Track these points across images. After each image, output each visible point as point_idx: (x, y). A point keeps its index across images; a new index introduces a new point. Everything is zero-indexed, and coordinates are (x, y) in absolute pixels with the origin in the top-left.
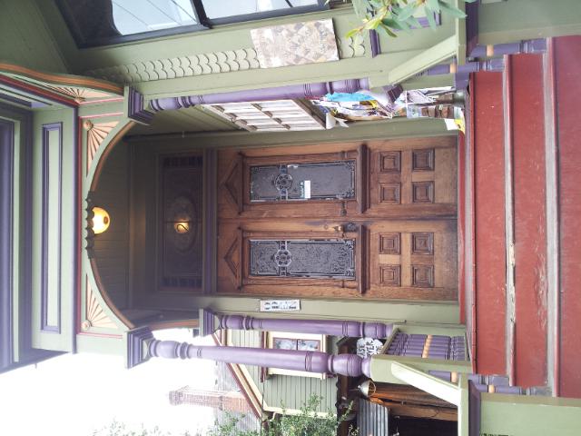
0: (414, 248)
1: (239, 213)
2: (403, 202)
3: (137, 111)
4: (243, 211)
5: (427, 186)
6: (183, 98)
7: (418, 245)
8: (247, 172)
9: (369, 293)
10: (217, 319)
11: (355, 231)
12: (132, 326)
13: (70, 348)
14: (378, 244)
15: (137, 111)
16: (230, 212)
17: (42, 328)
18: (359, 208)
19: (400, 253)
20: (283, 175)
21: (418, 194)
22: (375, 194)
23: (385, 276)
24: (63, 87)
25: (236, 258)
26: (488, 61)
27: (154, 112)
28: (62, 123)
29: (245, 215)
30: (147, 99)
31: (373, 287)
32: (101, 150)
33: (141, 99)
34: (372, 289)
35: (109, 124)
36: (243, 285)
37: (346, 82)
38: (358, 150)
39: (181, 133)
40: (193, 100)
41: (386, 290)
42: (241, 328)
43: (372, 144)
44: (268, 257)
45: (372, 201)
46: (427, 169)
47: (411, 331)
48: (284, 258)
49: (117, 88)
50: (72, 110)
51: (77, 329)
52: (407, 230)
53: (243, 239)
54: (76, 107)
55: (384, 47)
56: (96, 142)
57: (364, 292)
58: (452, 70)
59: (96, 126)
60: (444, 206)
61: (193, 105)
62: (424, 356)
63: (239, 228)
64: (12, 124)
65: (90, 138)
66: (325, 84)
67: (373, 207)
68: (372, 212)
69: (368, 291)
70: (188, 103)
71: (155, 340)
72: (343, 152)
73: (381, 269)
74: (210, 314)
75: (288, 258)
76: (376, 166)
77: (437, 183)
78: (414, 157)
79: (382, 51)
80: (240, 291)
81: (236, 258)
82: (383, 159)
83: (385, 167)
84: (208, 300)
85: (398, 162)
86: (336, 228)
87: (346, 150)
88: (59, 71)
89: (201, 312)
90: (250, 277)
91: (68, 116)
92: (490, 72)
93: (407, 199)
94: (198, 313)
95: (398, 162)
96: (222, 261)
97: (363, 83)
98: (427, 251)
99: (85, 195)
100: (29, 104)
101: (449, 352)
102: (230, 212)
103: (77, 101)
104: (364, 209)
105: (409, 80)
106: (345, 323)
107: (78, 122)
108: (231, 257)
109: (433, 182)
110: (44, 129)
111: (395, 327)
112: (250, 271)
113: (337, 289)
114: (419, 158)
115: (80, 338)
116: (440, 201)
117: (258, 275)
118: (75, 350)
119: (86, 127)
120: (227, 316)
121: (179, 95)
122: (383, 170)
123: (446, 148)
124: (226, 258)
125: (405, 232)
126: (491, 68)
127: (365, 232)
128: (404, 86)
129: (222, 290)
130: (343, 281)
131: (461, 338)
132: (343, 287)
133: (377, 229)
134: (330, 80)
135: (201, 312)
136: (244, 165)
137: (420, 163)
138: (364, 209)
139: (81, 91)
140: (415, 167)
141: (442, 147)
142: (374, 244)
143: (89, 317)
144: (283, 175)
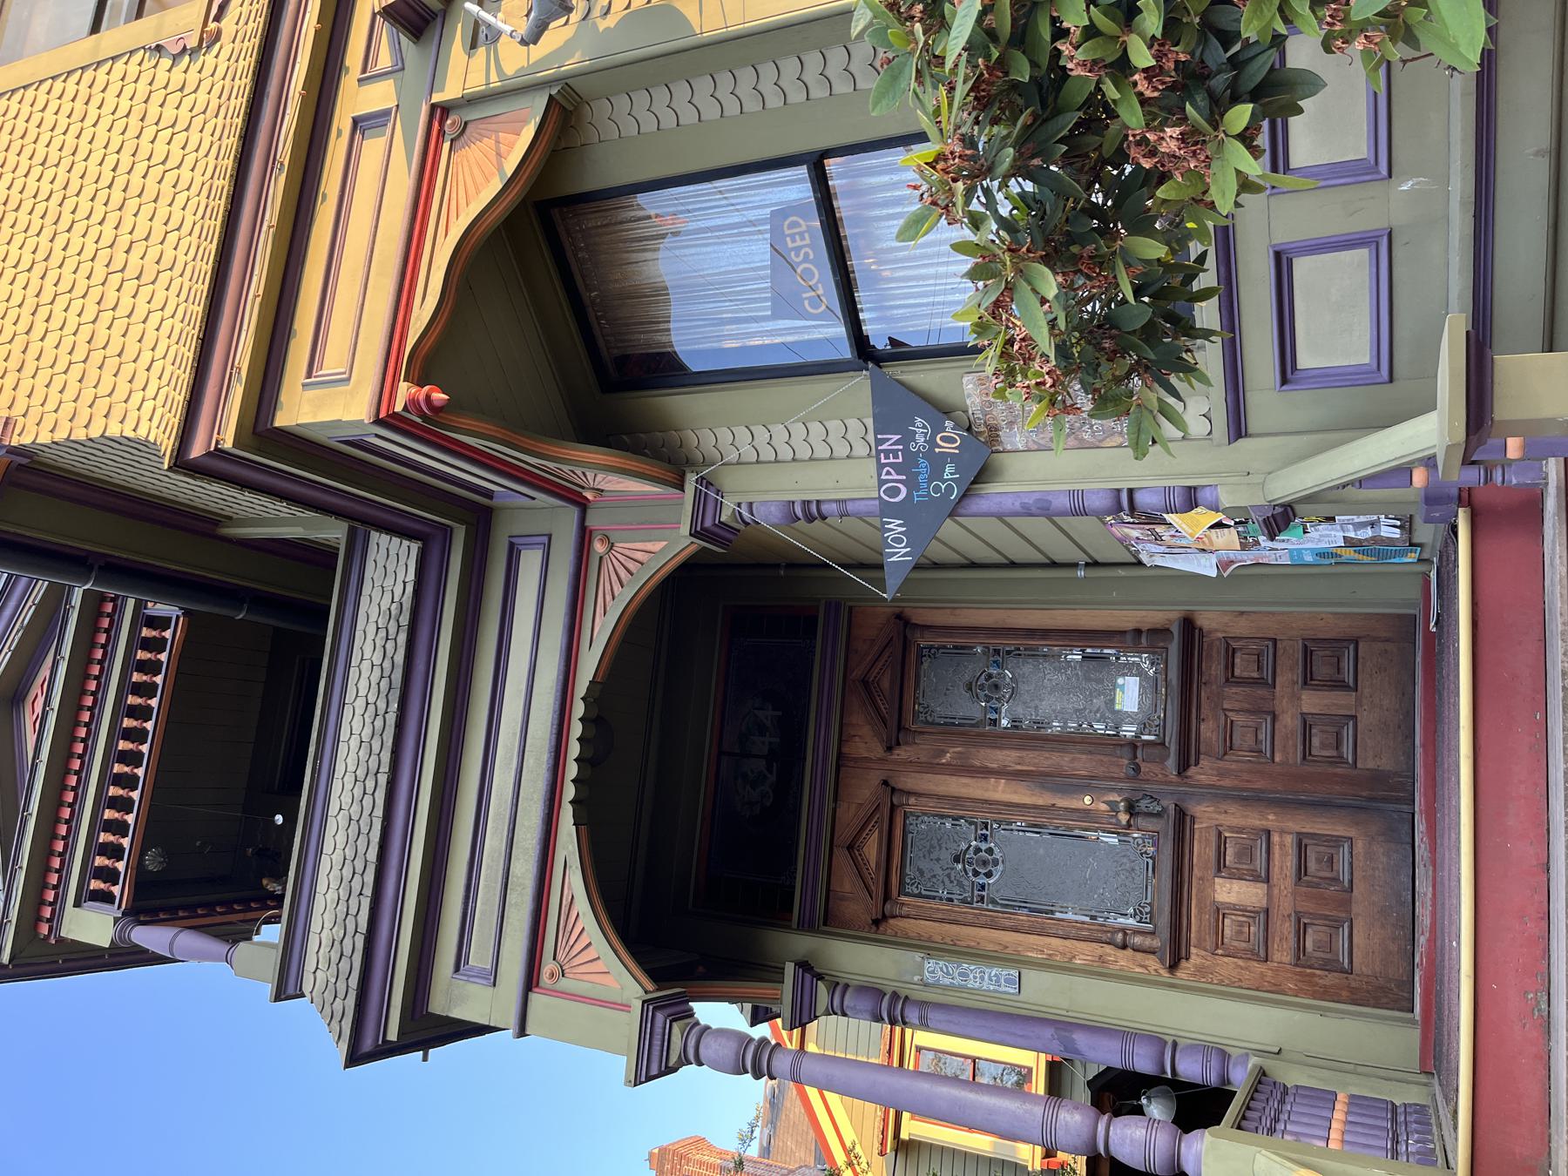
0: (1301, 869)
1: (889, 749)
2: (1277, 759)
3: (708, 523)
4: (898, 744)
5: (1338, 722)
6: (806, 503)
7: (1312, 865)
8: (913, 657)
9: (1185, 972)
10: (822, 989)
11: (1158, 815)
12: (650, 986)
13: (512, 1020)
14: (1211, 853)
15: (708, 523)
16: (866, 744)
17: (457, 969)
18: (1171, 763)
19: (1267, 880)
20: (994, 671)
21: (1316, 741)
22: (1208, 731)
23: (1227, 932)
24: (566, 468)
25: (871, 849)
26: (1506, 464)
27: (741, 527)
28: (550, 537)
29: (902, 753)
30: (729, 505)
31: (1196, 957)
32: (625, 595)
33: (719, 506)
34: (1194, 960)
35: (649, 546)
36: (885, 918)
37: (1167, 490)
38: (1175, 630)
39: (777, 566)
40: (825, 508)
41: (1227, 966)
42: (878, 1018)
43: (1206, 620)
44: (946, 856)
45: (1203, 749)
46: (1338, 685)
47: (1293, 1077)
48: (985, 863)
49: (669, 476)
50: (573, 513)
51: (531, 981)
52: (1286, 828)
53: (893, 808)
54: (583, 505)
55: (1255, 421)
56: (614, 577)
57: (1173, 967)
58: (1419, 477)
59: (619, 546)
60: (1377, 777)
61: (824, 518)
62: (1333, 1145)
63: (885, 783)
64: (447, 533)
65: (604, 568)
66: (1119, 491)
67: (1204, 762)
68: (1203, 773)
69: (1184, 963)
70: (813, 512)
71: (697, 1023)
72: (1138, 632)
73: (1220, 912)
74: (808, 976)
75: (996, 862)
76: (1215, 669)
77: (1366, 718)
78: (1307, 654)
79: (1250, 431)
80: (878, 926)
81: (871, 849)
82: (1231, 653)
83: (1237, 672)
84: (803, 943)
85: (1267, 661)
86: (1111, 804)
87: (1144, 629)
88: (560, 435)
89: (790, 968)
90: (903, 898)
91: (568, 517)
92: (1509, 488)
93: (1287, 753)
94: (782, 970)
95: (1267, 661)
96: (841, 857)
97: (1201, 495)
98: (1336, 880)
99: (581, 688)
100: (489, 494)
101: (1396, 1141)
102: (866, 744)
103: (589, 495)
104: (1184, 765)
105: (1311, 499)
106: (1127, 1035)
107: (584, 537)
108: (860, 849)
109: (1354, 717)
110: (512, 545)
111: (1254, 1061)
112: (902, 883)
113: (1108, 949)
114: (1319, 655)
115: (536, 998)
116: (1371, 764)
117: (920, 896)
118: (522, 1032)
119: (599, 547)
120: (847, 986)
121: (798, 497)
122: (1231, 678)
123: (1387, 640)
124: (850, 848)
125: (1282, 832)
126: (1514, 481)
127: (1182, 821)
128: (1298, 508)
129: (828, 921)
130: (1124, 931)
131: (1420, 1110)
132: (1124, 947)
133: (1206, 816)
134: (1132, 485)
135: (790, 968)
136: (906, 644)
137: (1322, 670)
138: (1184, 765)
139: (600, 477)
140: (1308, 679)
141: (1375, 639)
142: (1202, 850)
143: (559, 956)
144: (994, 671)
